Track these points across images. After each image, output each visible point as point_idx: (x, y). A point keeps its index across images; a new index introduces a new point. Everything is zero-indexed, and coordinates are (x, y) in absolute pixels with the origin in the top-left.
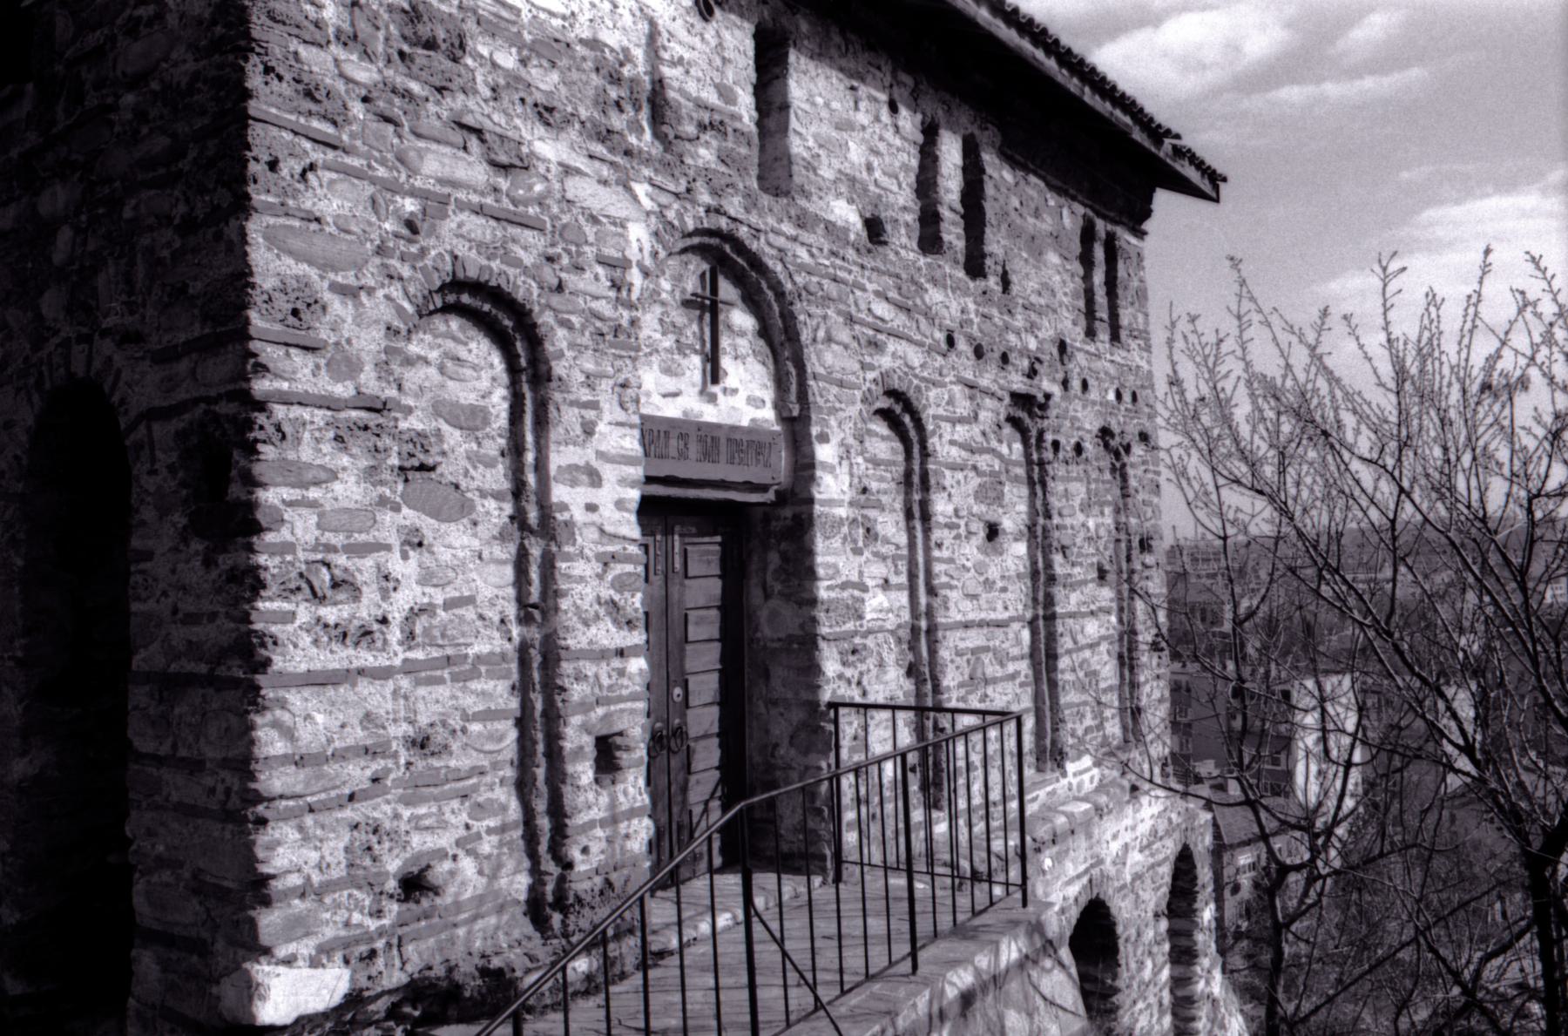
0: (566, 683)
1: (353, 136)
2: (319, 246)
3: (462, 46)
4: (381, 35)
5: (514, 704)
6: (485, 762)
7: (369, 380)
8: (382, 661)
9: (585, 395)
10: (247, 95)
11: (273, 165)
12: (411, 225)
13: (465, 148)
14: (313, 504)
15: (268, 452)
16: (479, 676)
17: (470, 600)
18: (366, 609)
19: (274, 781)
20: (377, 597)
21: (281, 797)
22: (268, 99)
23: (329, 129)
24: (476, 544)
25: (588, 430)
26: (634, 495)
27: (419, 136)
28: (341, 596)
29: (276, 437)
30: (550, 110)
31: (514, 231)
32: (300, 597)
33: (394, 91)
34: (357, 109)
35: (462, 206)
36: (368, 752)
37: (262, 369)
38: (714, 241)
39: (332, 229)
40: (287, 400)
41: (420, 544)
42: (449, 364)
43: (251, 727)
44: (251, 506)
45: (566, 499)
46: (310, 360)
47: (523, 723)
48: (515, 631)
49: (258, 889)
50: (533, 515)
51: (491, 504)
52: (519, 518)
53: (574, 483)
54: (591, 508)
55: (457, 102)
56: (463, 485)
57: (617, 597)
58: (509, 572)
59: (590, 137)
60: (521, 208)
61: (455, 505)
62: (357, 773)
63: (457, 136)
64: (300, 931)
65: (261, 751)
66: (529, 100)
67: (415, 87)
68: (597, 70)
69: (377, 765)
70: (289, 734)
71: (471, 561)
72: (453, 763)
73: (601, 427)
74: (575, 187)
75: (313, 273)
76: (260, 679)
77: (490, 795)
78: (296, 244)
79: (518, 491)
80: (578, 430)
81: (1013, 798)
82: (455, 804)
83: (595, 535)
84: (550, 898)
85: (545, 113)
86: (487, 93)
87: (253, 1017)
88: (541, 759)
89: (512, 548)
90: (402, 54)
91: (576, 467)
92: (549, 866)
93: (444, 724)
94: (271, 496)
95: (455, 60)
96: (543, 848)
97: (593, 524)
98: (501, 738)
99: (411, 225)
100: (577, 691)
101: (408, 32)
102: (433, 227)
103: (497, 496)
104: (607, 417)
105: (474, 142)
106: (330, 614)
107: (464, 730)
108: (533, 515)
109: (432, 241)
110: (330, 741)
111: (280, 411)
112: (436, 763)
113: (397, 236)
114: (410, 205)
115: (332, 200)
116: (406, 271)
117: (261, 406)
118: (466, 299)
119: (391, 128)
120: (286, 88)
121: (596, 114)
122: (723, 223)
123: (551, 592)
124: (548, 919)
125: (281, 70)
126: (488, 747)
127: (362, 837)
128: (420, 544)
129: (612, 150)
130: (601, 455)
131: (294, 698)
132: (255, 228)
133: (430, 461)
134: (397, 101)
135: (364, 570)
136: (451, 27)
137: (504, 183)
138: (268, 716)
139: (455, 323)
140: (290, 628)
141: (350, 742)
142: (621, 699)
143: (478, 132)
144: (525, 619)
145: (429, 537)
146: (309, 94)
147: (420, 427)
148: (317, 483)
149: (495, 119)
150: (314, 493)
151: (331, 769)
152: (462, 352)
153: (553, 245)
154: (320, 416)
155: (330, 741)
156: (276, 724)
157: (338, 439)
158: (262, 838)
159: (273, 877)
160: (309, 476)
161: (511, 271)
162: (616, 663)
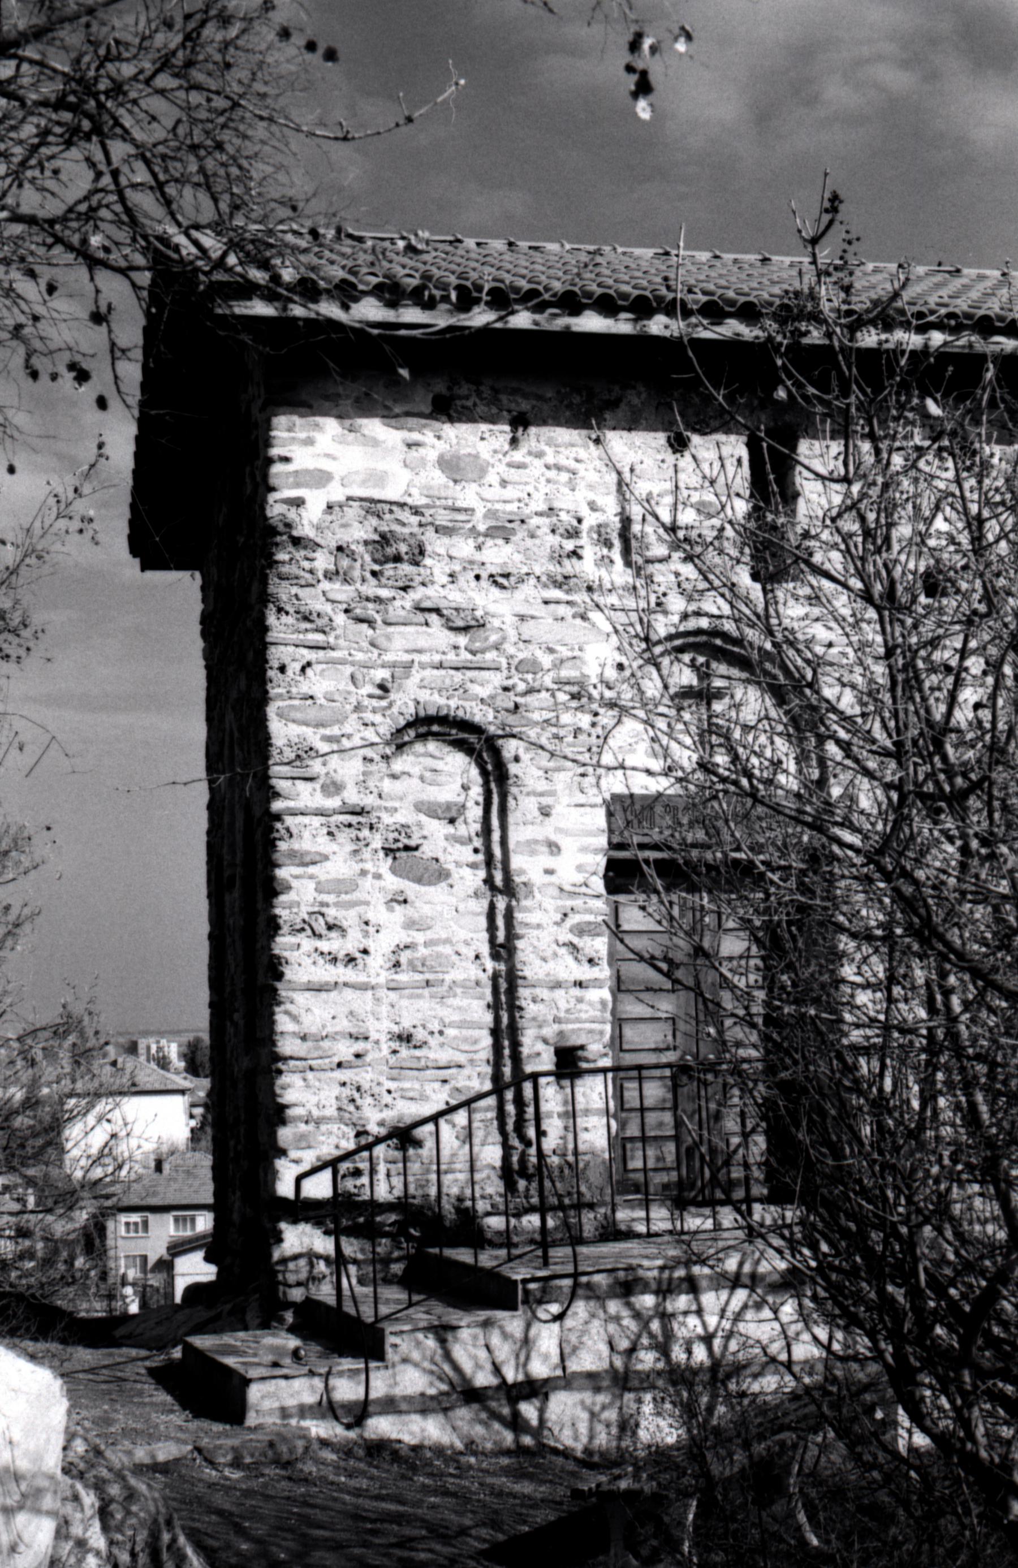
0: (523, 1003)
1: (337, 638)
2: (312, 714)
3: (422, 553)
4: (358, 564)
5: (488, 1018)
6: (462, 1058)
7: (352, 796)
8: (362, 978)
9: (542, 786)
10: (266, 629)
11: (282, 669)
12: (383, 687)
13: (427, 624)
14: (311, 877)
15: (282, 846)
16: (455, 996)
17: (447, 941)
18: (350, 945)
19: (287, 1046)
20: (360, 935)
21: (291, 1058)
22: (280, 627)
23: (319, 637)
24: (454, 900)
25: (545, 812)
26: (602, 861)
27: (390, 624)
28: (333, 934)
29: (286, 836)
30: (507, 576)
31: (470, 674)
32: (303, 935)
33: (368, 599)
34: (340, 619)
35: (423, 666)
36: (354, 1037)
37: (277, 795)
38: (703, 638)
39: (323, 701)
40: (294, 813)
41: (405, 901)
42: (428, 775)
43: (273, 1014)
44: (272, 879)
45: (525, 866)
46: (309, 785)
47: (495, 1032)
48: (490, 965)
49: (279, 1114)
50: (498, 878)
51: (467, 872)
52: (489, 881)
53: (533, 853)
54: (549, 872)
55: (416, 595)
56: (442, 859)
57: (576, 940)
58: (483, 922)
59: (545, 586)
60: (479, 656)
61: (436, 874)
62: (345, 1050)
63: (420, 617)
64: (304, 1144)
65: (279, 1028)
66: (484, 575)
67: (384, 593)
68: (553, 531)
69: (360, 1046)
70: (295, 1019)
71: (454, 914)
72: (432, 1055)
73: (557, 810)
74: (528, 629)
75: (308, 731)
76: (279, 985)
77: (468, 1083)
78: (298, 716)
79: (489, 862)
80: (537, 813)
81: (508, 1086)
82: (437, 1085)
83: (556, 892)
84: (516, 1166)
85: (501, 580)
86: (445, 579)
87: (274, 1191)
88: (508, 1062)
89: (485, 904)
90: (374, 574)
91: (536, 842)
92: (515, 1142)
93: (424, 1027)
94: (283, 873)
95: (417, 564)
96: (510, 1127)
97: (550, 884)
98: (476, 1042)
99: (383, 687)
100: (531, 1009)
101: (378, 556)
102: (400, 686)
103: (473, 866)
104: (565, 800)
105: (433, 618)
106: (324, 946)
107: (441, 1033)
108: (498, 878)
109: (401, 695)
110: (324, 1026)
111: (289, 821)
112: (417, 1053)
113: (371, 696)
114: (381, 674)
115: (319, 683)
116: (378, 718)
117: (278, 817)
118: (435, 728)
119: (365, 626)
120: (289, 620)
121: (551, 568)
122: (704, 623)
123: (511, 935)
124: (515, 1183)
125: (288, 608)
126: (467, 1048)
127: (347, 1092)
128: (405, 901)
129: (568, 592)
130: (558, 830)
131: (302, 999)
132: (271, 710)
133: (413, 843)
134: (370, 605)
135: (349, 918)
136: (412, 542)
137: (462, 640)
138: (282, 1008)
139: (432, 746)
140: (296, 953)
141: (338, 1029)
142: (578, 1020)
143: (437, 611)
144: (495, 956)
145: (411, 897)
146: (306, 619)
147: (403, 821)
148: (314, 863)
149: (454, 596)
150: (311, 870)
151: (326, 1044)
152: (439, 765)
153: (509, 678)
154: (317, 821)
155: (324, 1026)
156: (287, 1013)
157: (330, 834)
158: (284, 1079)
159: (287, 1107)
160: (307, 859)
161: (467, 704)
162: (576, 992)
